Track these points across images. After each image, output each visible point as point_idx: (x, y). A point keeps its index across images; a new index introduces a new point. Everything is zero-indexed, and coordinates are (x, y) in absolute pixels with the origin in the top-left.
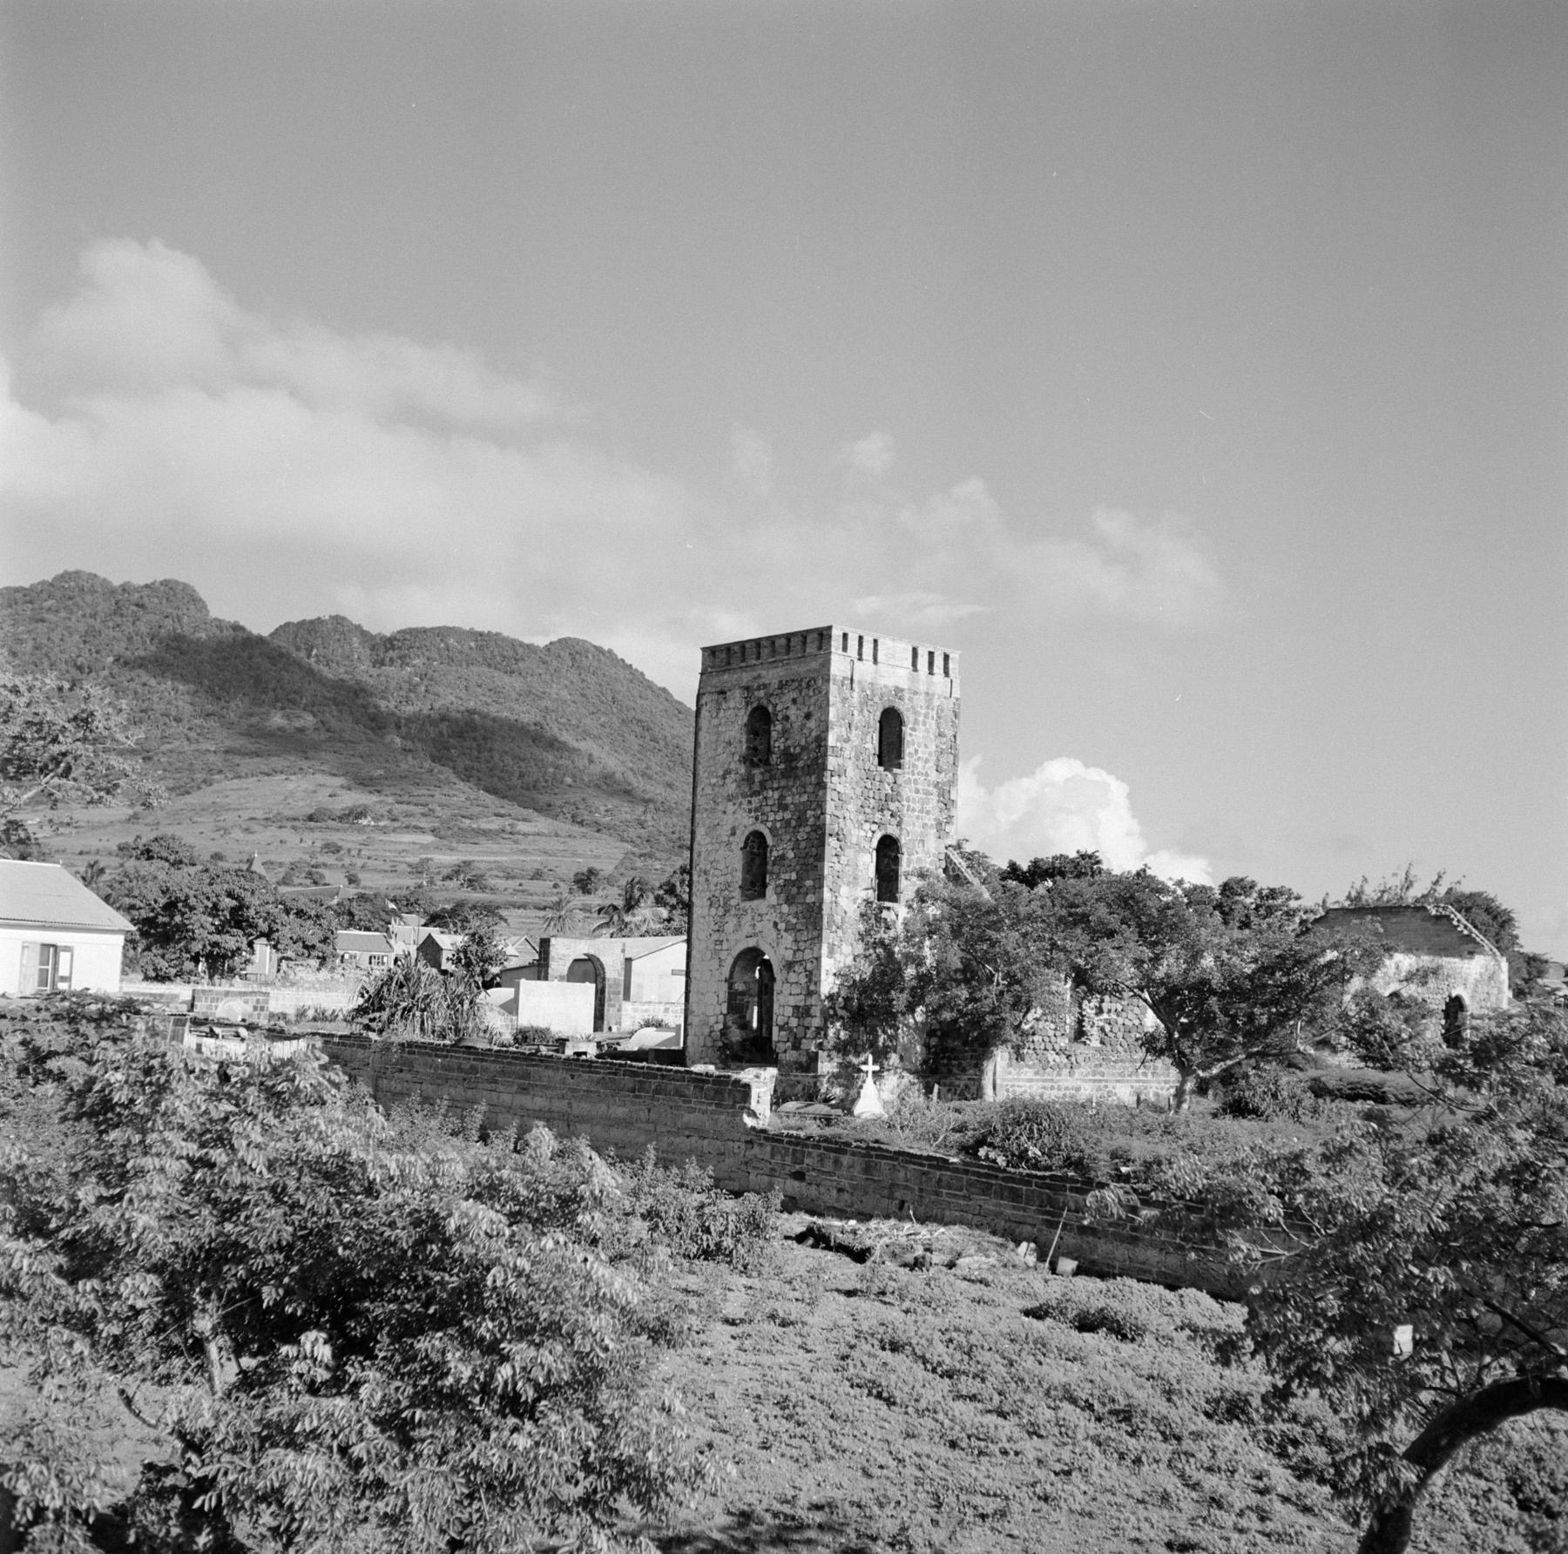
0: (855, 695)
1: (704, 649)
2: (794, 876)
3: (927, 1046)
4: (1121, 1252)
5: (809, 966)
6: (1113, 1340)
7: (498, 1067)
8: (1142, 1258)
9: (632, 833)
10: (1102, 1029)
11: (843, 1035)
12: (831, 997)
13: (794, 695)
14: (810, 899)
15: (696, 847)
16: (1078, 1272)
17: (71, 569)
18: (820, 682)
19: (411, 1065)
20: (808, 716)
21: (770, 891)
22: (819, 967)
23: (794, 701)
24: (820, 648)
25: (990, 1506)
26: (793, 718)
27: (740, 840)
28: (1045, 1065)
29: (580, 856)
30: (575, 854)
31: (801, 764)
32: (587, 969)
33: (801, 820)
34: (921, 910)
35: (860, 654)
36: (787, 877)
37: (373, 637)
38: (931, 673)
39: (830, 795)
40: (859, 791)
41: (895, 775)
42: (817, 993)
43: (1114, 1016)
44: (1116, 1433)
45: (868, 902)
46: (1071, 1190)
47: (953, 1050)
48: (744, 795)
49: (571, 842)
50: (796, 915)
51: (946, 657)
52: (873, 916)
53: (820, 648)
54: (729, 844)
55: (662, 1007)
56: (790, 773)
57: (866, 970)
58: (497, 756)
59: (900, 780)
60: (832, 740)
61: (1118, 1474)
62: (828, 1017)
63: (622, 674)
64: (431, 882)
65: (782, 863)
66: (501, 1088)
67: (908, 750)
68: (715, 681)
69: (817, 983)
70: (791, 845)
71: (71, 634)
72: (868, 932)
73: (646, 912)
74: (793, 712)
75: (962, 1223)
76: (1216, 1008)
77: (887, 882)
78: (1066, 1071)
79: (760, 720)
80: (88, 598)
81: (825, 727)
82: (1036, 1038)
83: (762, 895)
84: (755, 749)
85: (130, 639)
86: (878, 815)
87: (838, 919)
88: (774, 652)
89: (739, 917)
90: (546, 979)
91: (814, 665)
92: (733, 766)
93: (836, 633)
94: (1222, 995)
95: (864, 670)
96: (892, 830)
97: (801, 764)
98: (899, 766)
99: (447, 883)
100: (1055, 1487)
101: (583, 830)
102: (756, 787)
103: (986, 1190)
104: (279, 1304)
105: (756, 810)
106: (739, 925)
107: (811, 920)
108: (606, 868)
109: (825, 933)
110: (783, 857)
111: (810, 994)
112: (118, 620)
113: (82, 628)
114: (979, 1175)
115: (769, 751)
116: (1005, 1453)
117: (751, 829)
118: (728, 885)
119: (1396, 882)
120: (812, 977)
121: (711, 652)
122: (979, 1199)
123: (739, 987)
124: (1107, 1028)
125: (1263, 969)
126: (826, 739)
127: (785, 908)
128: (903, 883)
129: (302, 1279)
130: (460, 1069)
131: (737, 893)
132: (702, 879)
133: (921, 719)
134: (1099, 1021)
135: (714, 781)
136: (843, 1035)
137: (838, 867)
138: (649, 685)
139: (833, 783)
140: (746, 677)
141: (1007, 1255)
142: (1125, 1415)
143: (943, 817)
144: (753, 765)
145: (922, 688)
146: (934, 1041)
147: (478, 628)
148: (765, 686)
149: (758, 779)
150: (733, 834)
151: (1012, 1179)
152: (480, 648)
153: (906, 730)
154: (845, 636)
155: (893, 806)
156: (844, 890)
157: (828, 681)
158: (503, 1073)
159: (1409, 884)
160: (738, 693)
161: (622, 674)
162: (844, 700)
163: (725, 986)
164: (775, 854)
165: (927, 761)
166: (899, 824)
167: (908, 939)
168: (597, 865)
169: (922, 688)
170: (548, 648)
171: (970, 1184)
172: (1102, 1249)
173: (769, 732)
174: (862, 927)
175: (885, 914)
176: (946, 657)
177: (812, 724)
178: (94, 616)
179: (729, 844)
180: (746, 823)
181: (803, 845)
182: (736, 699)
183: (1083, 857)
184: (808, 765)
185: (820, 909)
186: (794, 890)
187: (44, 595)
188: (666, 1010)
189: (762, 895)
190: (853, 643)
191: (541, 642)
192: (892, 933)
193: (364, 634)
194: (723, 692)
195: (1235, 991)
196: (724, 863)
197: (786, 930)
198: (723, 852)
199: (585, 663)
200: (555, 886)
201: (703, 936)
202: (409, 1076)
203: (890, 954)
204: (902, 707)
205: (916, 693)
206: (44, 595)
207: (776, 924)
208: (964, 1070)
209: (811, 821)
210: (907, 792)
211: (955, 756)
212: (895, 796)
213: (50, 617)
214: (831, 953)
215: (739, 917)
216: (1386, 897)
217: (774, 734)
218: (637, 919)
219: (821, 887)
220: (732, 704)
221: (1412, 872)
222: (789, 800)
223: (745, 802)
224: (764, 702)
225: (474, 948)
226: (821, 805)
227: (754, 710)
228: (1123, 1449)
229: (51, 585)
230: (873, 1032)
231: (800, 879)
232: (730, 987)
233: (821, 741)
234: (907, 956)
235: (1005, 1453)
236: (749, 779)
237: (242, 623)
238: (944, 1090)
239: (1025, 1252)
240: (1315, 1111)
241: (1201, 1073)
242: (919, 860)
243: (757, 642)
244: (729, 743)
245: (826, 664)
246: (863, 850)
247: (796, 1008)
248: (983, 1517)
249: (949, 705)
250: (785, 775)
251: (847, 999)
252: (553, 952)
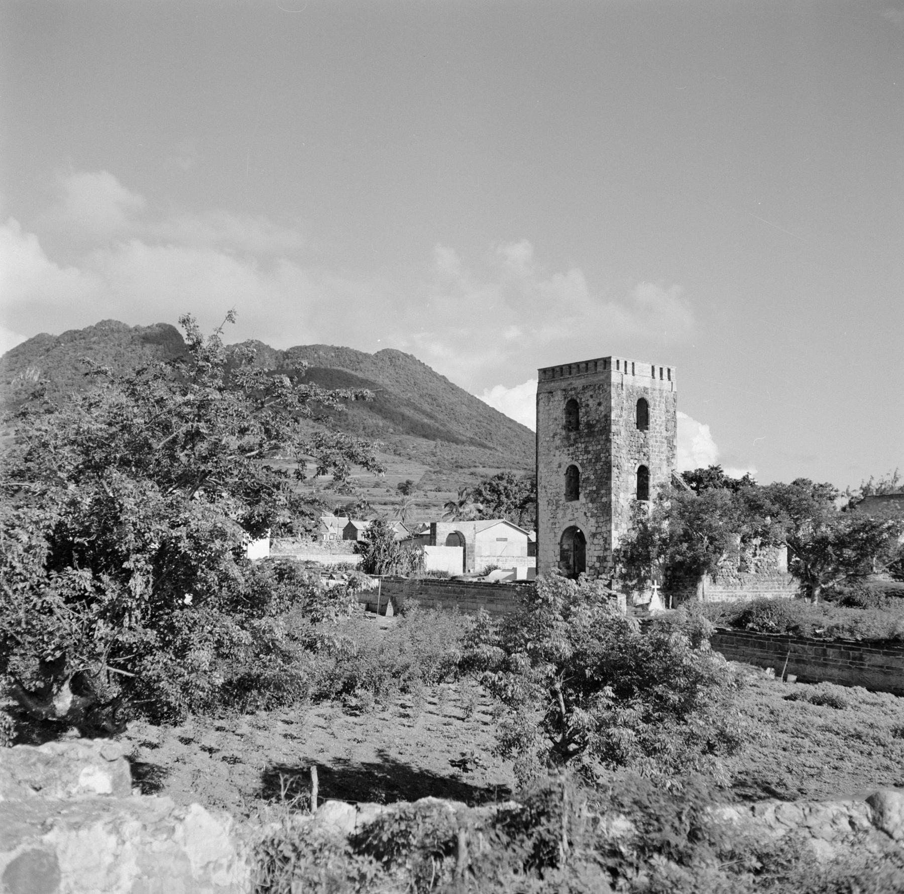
0: (624, 392)
1: (539, 370)
2: (594, 488)
3: (665, 575)
4: (819, 671)
5: (605, 535)
6: (831, 709)
7: (476, 590)
8: (829, 673)
9: (429, 459)
10: (756, 565)
11: (624, 571)
12: (617, 550)
13: (591, 393)
14: (604, 500)
15: (539, 474)
16: (798, 680)
17: (106, 319)
18: (605, 386)
19: (426, 591)
20: (600, 404)
21: (581, 496)
22: (610, 536)
23: (591, 396)
24: (605, 368)
25: (813, 771)
26: (591, 405)
27: (564, 470)
28: (728, 584)
29: (401, 473)
30: (397, 472)
31: (596, 429)
32: (456, 539)
33: (598, 459)
34: (661, 504)
35: (626, 371)
37: (276, 352)
38: (662, 379)
39: (613, 445)
40: (627, 442)
41: (645, 434)
42: (610, 549)
43: (762, 557)
44: (857, 743)
45: (634, 501)
46: (792, 642)
47: (679, 577)
48: (565, 446)
49: (395, 466)
50: (597, 509)
51: (669, 370)
52: (637, 508)
53: (605, 368)
54: (557, 472)
55: (495, 559)
56: (591, 434)
57: (634, 535)
58: (350, 418)
59: (648, 436)
60: (613, 417)
61: (863, 759)
62: (616, 562)
63: (419, 368)
64: (318, 491)
65: (588, 481)
66: (478, 601)
67: (651, 420)
68: (546, 387)
69: (610, 544)
70: (592, 472)
71: (107, 356)
72: (635, 516)
73: (471, 507)
74: (591, 402)
75: (735, 660)
76: (831, 552)
77: (642, 491)
78: (739, 587)
79: (573, 407)
80: (116, 335)
81: (609, 409)
82: (723, 570)
83: (578, 499)
84: (570, 422)
85: (140, 358)
86: (637, 456)
87: (619, 510)
88: (579, 371)
90: (435, 545)
91: (602, 377)
92: (558, 431)
93: (613, 360)
94: (834, 545)
95: (628, 379)
96: (645, 463)
97: (596, 429)
98: (647, 429)
99: (327, 491)
100: (839, 764)
101: (401, 458)
102: (572, 442)
103: (746, 643)
104: (592, 677)
105: (572, 454)
106: (565, 514)
107: (605, 511)
108: (416, 480)
109: (613, 517)
110: (588, 478)
111: (606, 550)
112: (133, 347)
113: (113, 352)
114: (742, 636)
115: (578, 423)
116: (809, 752)
117: (570, 464)
118: (558, 493)
119: (889, 479)
120: (607, 541)
121: (543, 372)
122: (743, 648)
123: (566, 547)
124: (759, 564)
125: (854, 531)
126: (610, 416)
127: (590, 505)
128: (651, 490)
129: (600, 668)
130: (454, 592)
131: (563, 498)
132: (543, 490)
134: (754, 560)
135: (548, 439)
136: (624, 571)
137: (618, 483)
138: (435, 375)
139: (614, 438)
140: (564, 385)
141: (762, 674)
142: (859, 737)
143: (670, 455)
144: (570, 430)
145: (657, 387)
146: (669, 573)
147: (336, 345)
148: (575, 389)
149: (572, 437)
150: (560, 467)
151: (760, 638)
152: (337, 356)
153: (650, 410)
154: (618, 361)
155: (645, 450)
156: (622, 495)
157: (610, 385)
158: (479, 593)
159: (896, 479)
160: (559, 393)
161: (419, 368)
162: (619, 395)
163: (559, 547)
166: (648, 459)
167: (655, 519)
168: (411, 479)
169: (657, 387)
170: (376, 355)
171: (738, 641)
172: (809, 670)
173: (578, 413)
174: (631, 514)
175: (642, 507)
176: (669, 370)
177: (602, 408)
178: (120, 345)
179: (557, 472)
180: (567, 461)
181: (599, 472)
182: (559, 396)
183: (712, 469)
184: (602, 430)
185: (610, 505)
186: (595, 496)
187: (91, 335)
188: (498, 560)
189: (577, 498)
190: (622, 365)
191: (372, 352)
192: (646, 517)
193: (272, 350)
194: (551, 392)
195: (841, 543)
196: (554, 482)
198: (555, 476)
199: (398, 363)
200: (388, 491)
201: (544, 520)
202: (426, 596)
203: (646, 528)
204: (648, 397)
205: (654, 390)
206: (91, 335)
207: (585, 514)
208: (686, 588)
209: (603, 459)
210: (651, 442)
211: (675, 422)
212: (645, 445)
213: (95, 346)
214: (616, 528)
216: (883, 487)
217: (581, 414)
218: (467, 510)
219: (610, 493)
220: (556, 398)
221: (898, 473)
222: (590, 448)
223: (566, 450)
224: (575, 397)
225: (376, 528)
226: (608, 451)
227: (569, 401)
228: (862, 749)
229: (95, 328)
230: (639, 569)
231: (598, 489)
232: (561, 547)
233: (607, 417)
234: (654, 528)
235: (809, 752)
236: (568, 438)
238: (675, 598)
239: (769, 672)
240: (888, 603)
241: (823, 586)
242: (659, 478)
243: (570, 366)
244: (556, 419)
245: (609, 377)
246: (630, 473)
247: (598, 557)
248: (812, 776)
249: (671, 395)
250: (588, 435)
251: (625, 552)
252: (438, 530)
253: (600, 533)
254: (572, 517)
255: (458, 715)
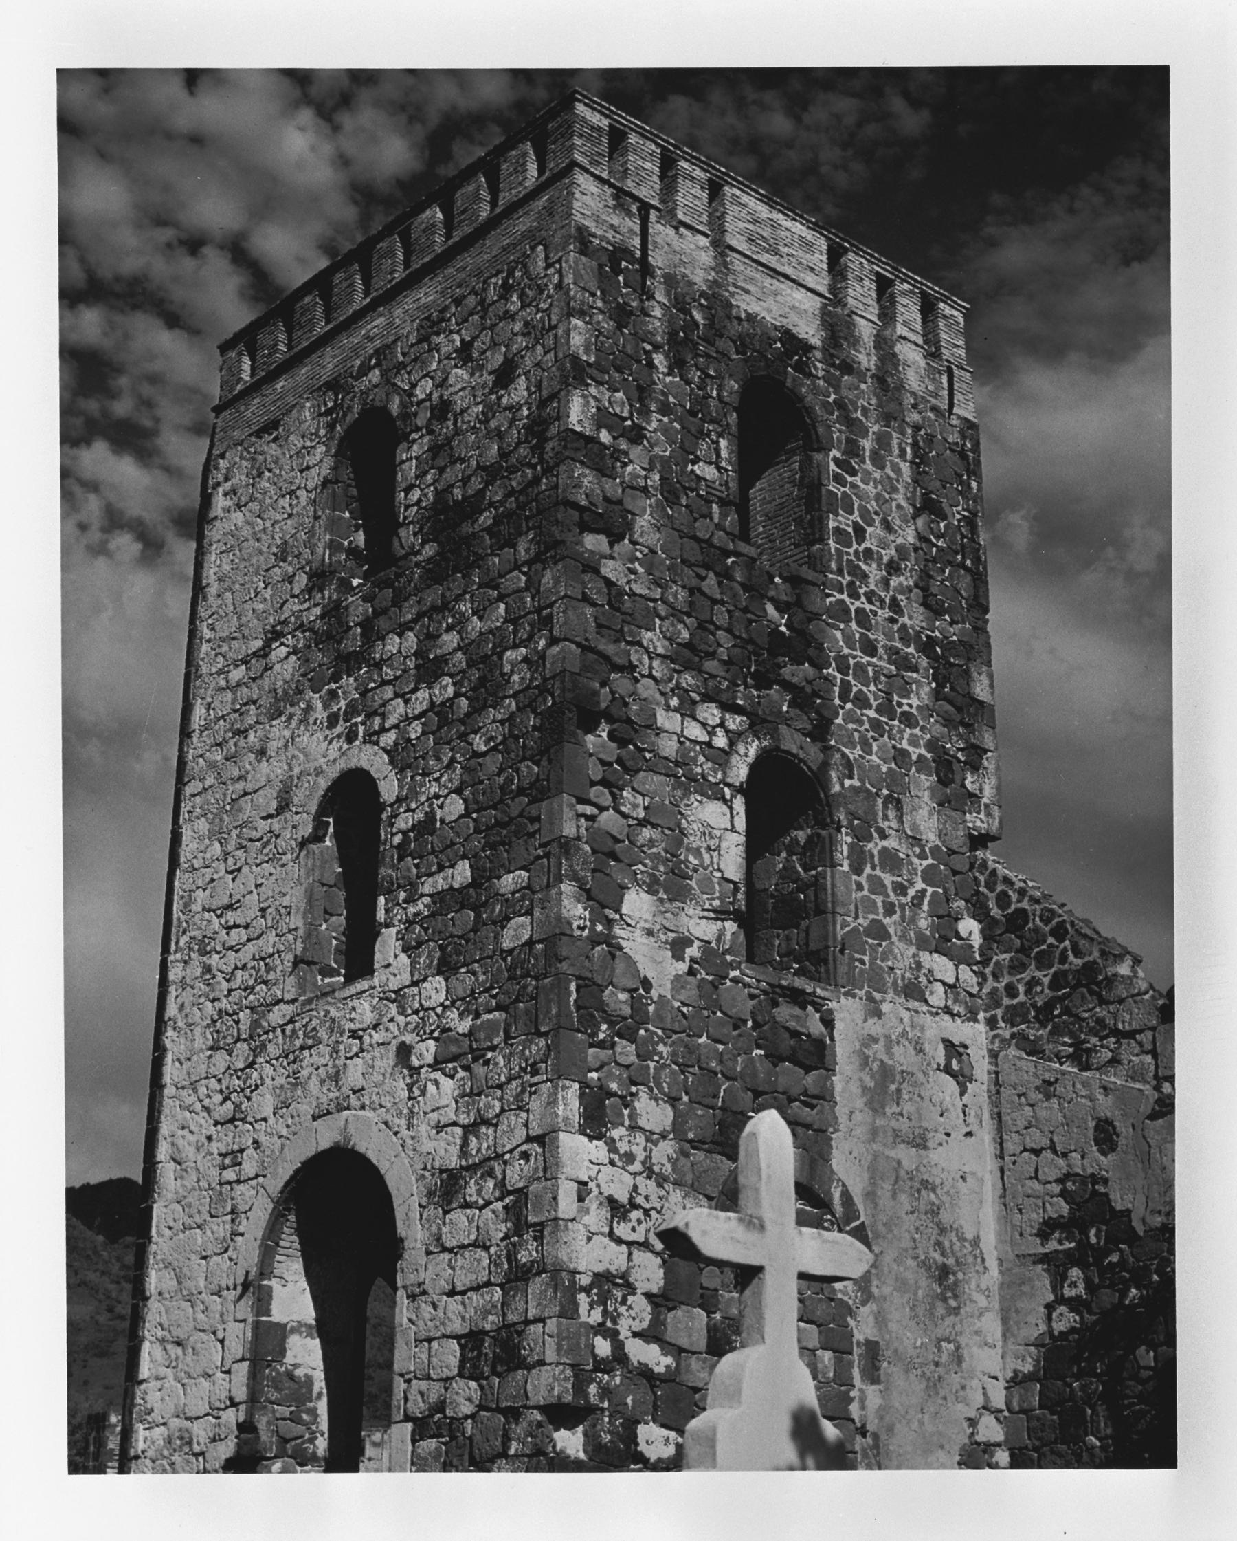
5: (516, 1174)
22: (549, 1171)
36: (437, 883)
50: (467, 1004)
89: (291, 1057)
111: (517, 1277)
127: (435, 990)
133: (867, 444)
156: (637, 903)
164: (405, 821)
165: (893, 568)
197: (437, 1065)
207: (404, 1051)
215: (291, 1057)
237: (616, 1196)
247: (471, 1340)
253: (483, 1168)
254: (327, 1095)
255: (947, 980)
